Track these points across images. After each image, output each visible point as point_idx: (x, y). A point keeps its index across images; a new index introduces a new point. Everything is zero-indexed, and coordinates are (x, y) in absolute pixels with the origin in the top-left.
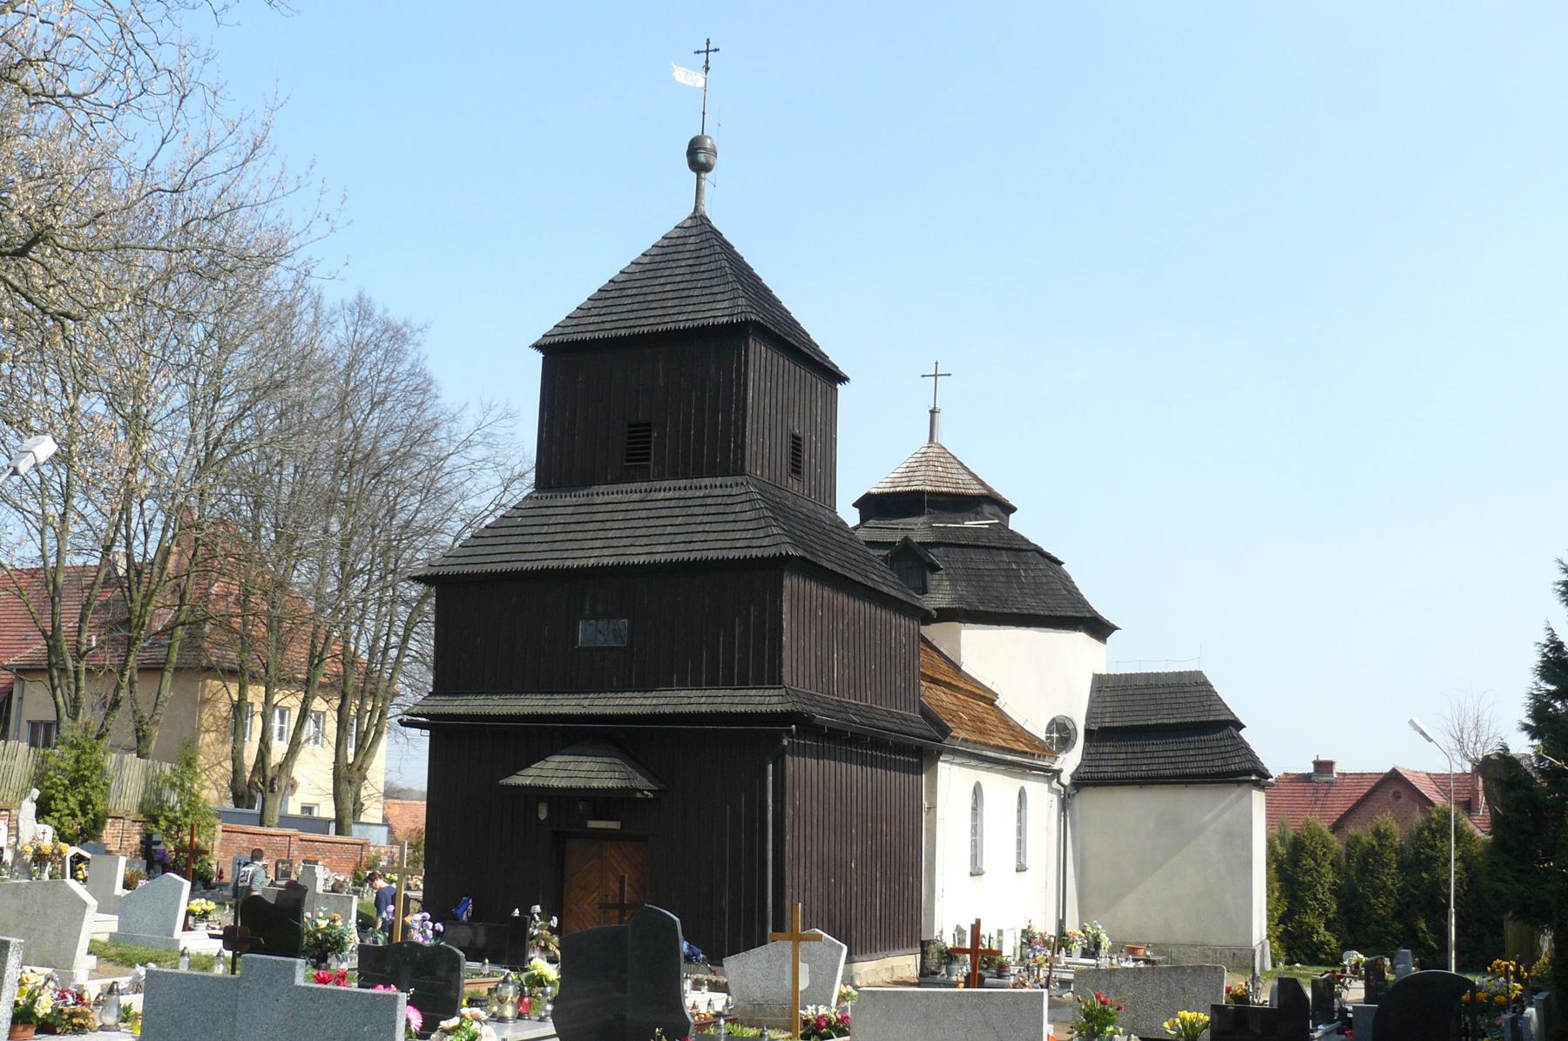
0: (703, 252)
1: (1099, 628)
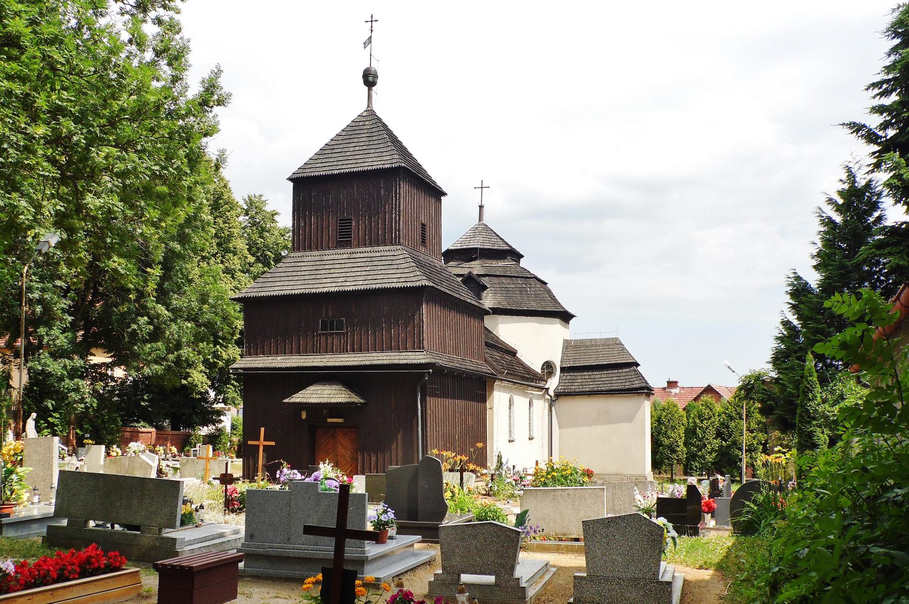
0: (374, 130)
1: (565, 317)
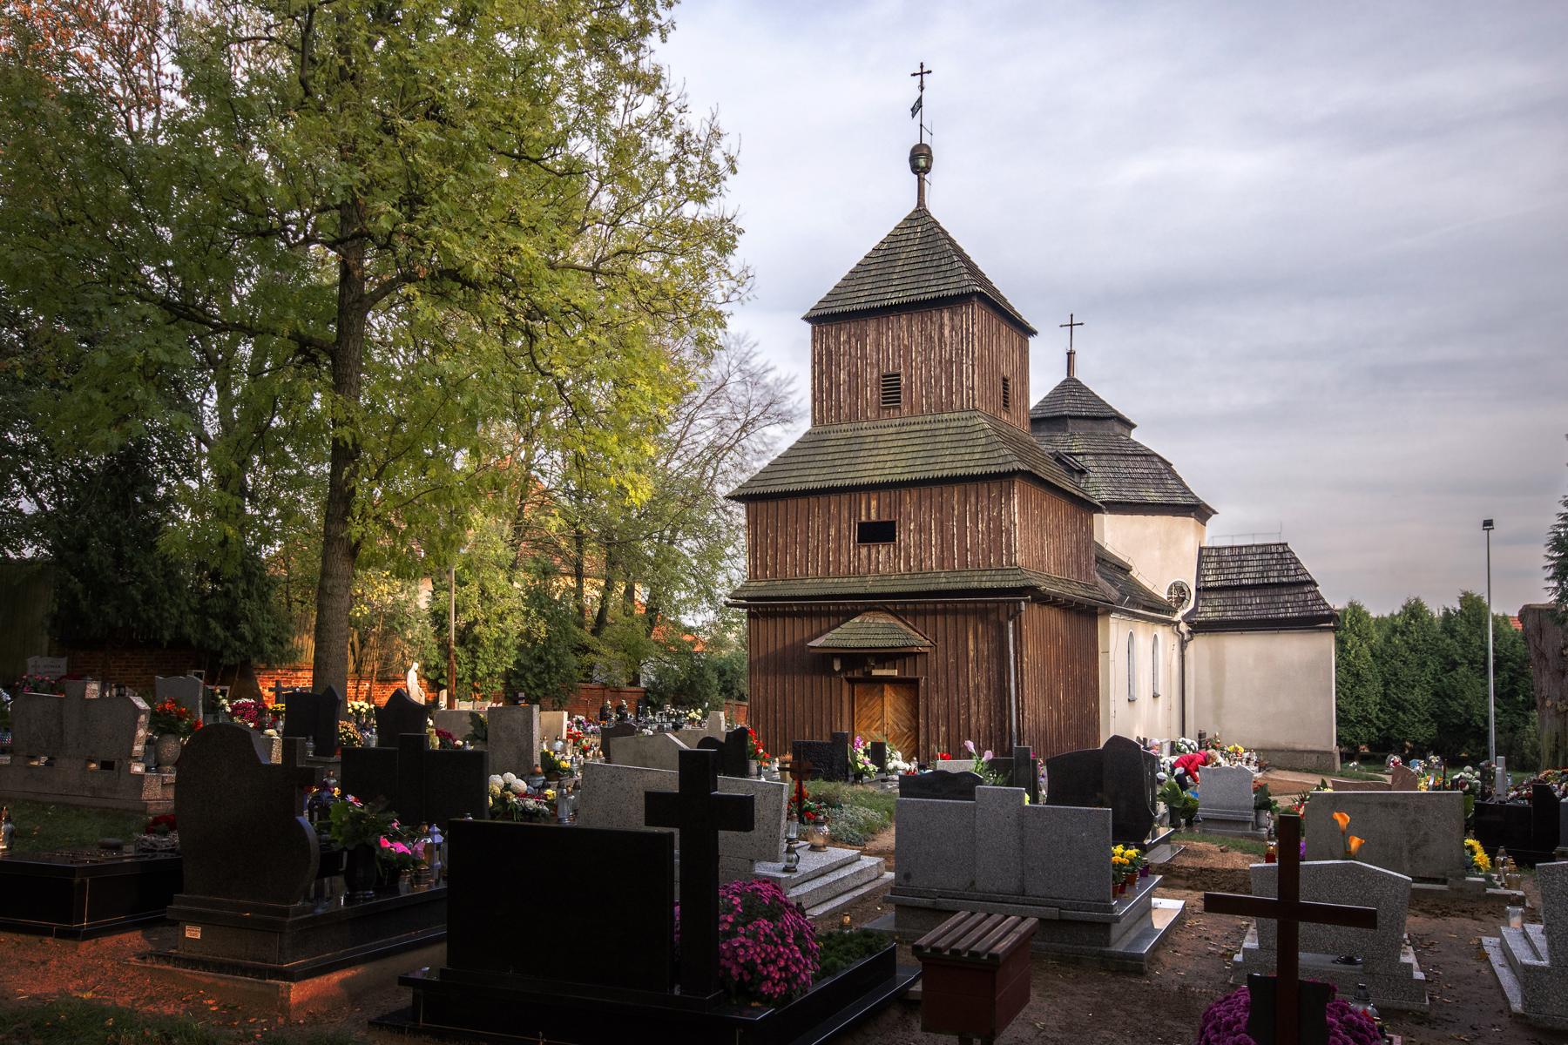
1: (1201, 512)
